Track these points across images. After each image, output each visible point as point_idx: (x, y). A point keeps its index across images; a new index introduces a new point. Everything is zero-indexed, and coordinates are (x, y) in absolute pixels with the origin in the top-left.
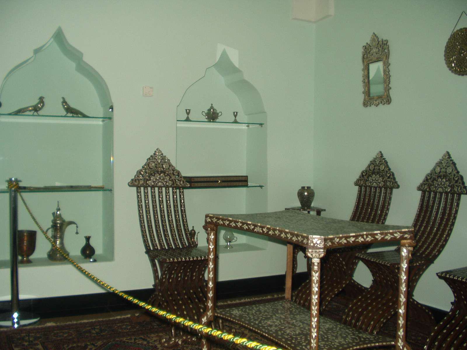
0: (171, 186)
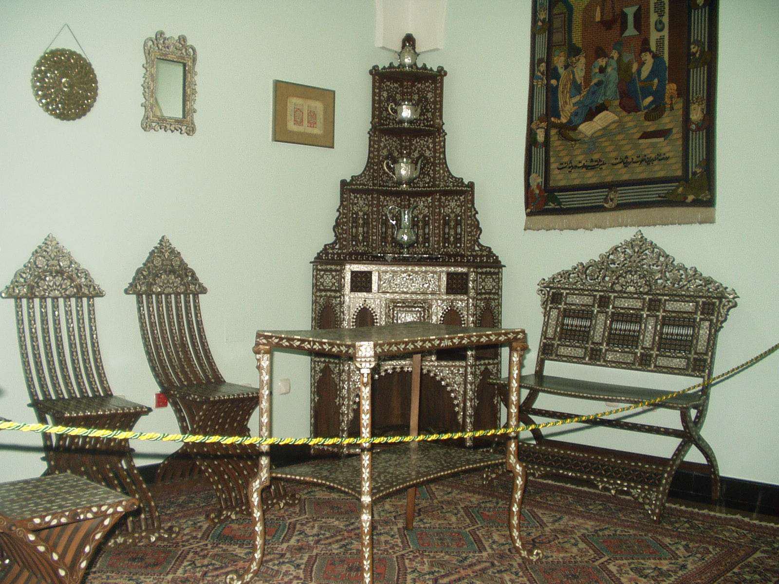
0: (182, 293)
